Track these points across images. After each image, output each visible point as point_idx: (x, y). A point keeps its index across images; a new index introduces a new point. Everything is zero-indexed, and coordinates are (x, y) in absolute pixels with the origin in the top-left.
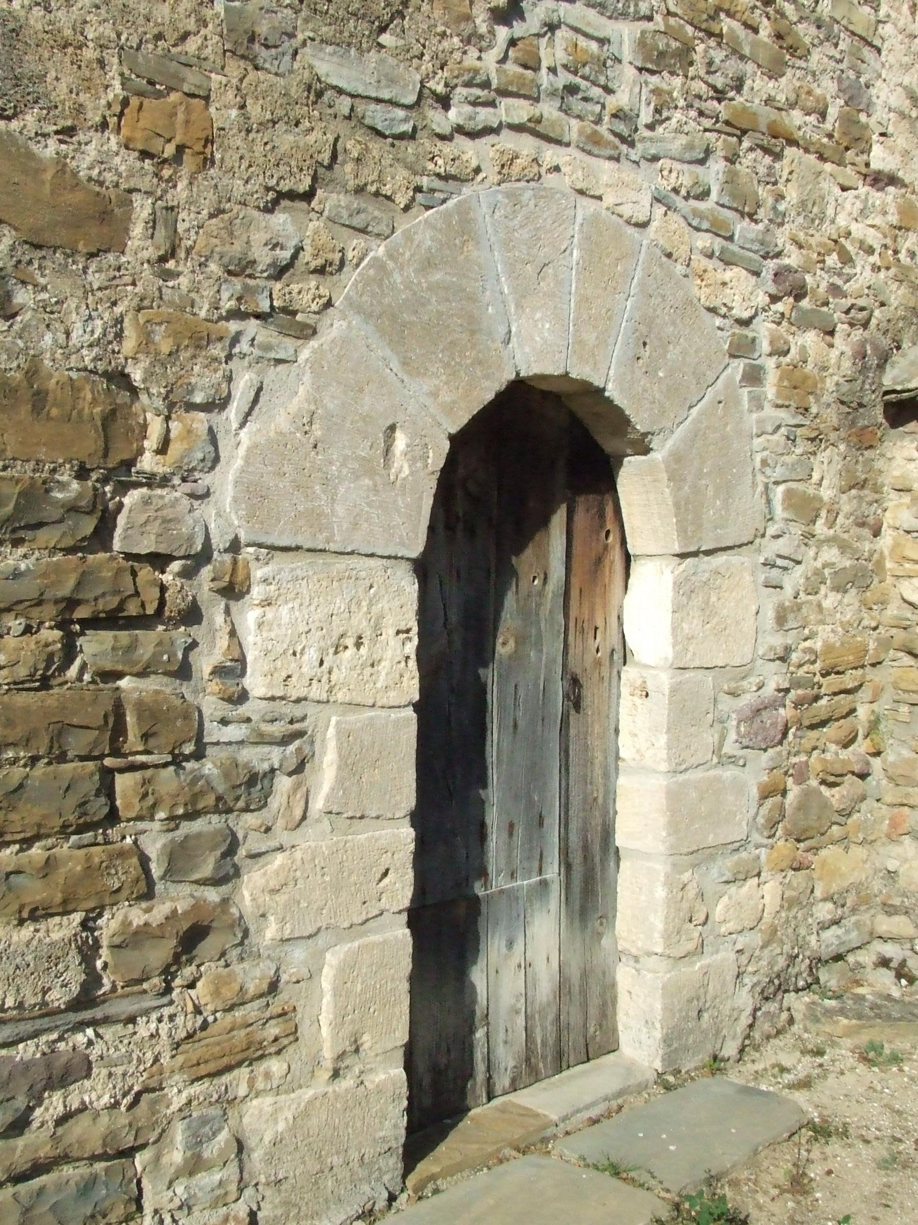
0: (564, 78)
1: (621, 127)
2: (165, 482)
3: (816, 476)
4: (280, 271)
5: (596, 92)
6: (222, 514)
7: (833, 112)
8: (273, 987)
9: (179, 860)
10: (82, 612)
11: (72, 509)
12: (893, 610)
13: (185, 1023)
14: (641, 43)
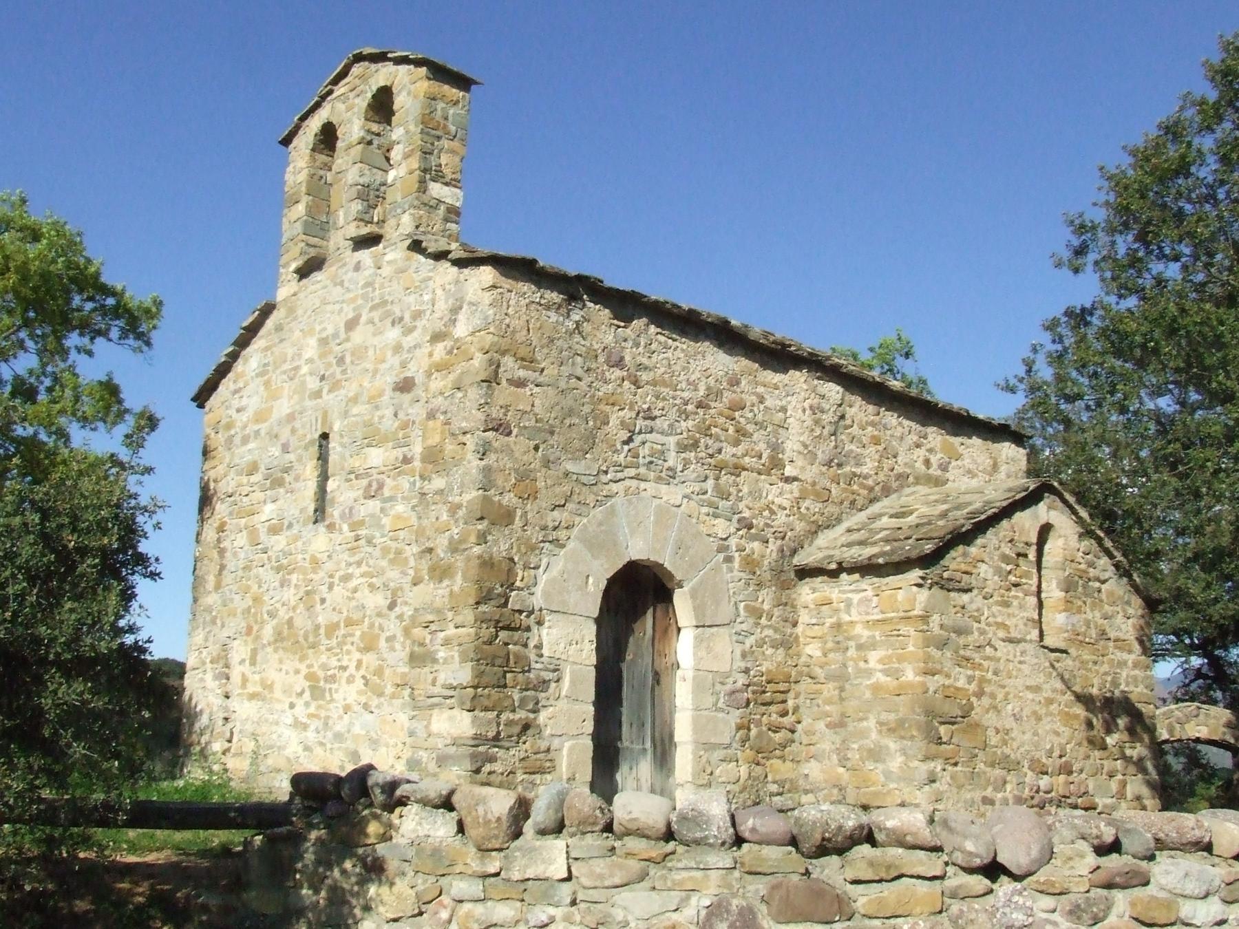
0: (648, 459)
1: (670, 473)
2: (522, 589)
3: (760, 600)
4: (555, 528)
5: (660, 462)
6: (537, 601)
7: (765, 456)
8: (548, 750)
9: (523, 701)
10: (500, 625)
11: (499, 595)
12: (803, 659)
13: (523, 755)
14: (678, 443)
